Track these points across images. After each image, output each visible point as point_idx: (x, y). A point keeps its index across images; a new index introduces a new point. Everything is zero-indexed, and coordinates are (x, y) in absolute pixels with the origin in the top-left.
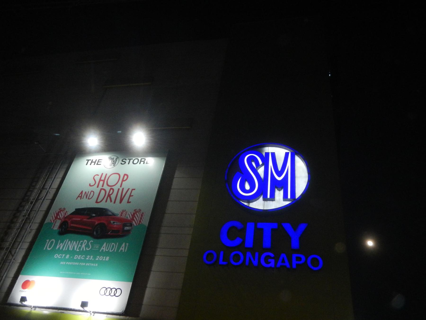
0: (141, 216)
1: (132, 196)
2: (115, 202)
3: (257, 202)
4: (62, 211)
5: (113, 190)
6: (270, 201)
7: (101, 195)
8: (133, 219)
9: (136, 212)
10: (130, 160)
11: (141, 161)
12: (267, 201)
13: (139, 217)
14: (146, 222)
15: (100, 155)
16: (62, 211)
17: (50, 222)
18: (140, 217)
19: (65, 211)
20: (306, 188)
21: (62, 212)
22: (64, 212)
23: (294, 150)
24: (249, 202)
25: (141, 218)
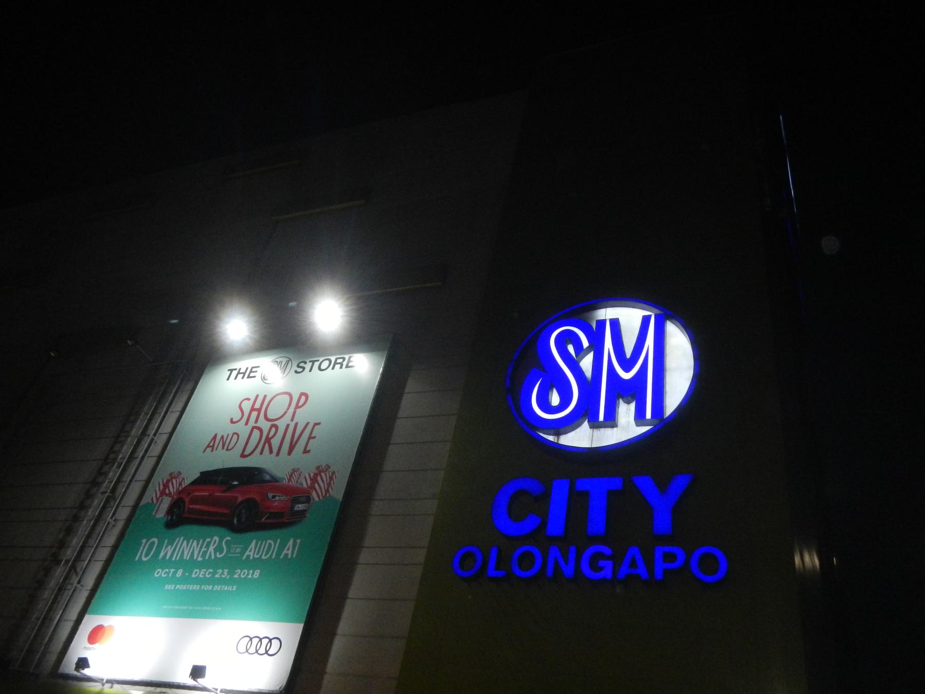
0: (330, 480)
1: (315, 437)
2: (278, 454)
5: (276, 427)
6: (606, 429)
7: (302, 436)
10: (313, 362)
11: (336, 363)
14: (338, 491)
25: (329, 485)
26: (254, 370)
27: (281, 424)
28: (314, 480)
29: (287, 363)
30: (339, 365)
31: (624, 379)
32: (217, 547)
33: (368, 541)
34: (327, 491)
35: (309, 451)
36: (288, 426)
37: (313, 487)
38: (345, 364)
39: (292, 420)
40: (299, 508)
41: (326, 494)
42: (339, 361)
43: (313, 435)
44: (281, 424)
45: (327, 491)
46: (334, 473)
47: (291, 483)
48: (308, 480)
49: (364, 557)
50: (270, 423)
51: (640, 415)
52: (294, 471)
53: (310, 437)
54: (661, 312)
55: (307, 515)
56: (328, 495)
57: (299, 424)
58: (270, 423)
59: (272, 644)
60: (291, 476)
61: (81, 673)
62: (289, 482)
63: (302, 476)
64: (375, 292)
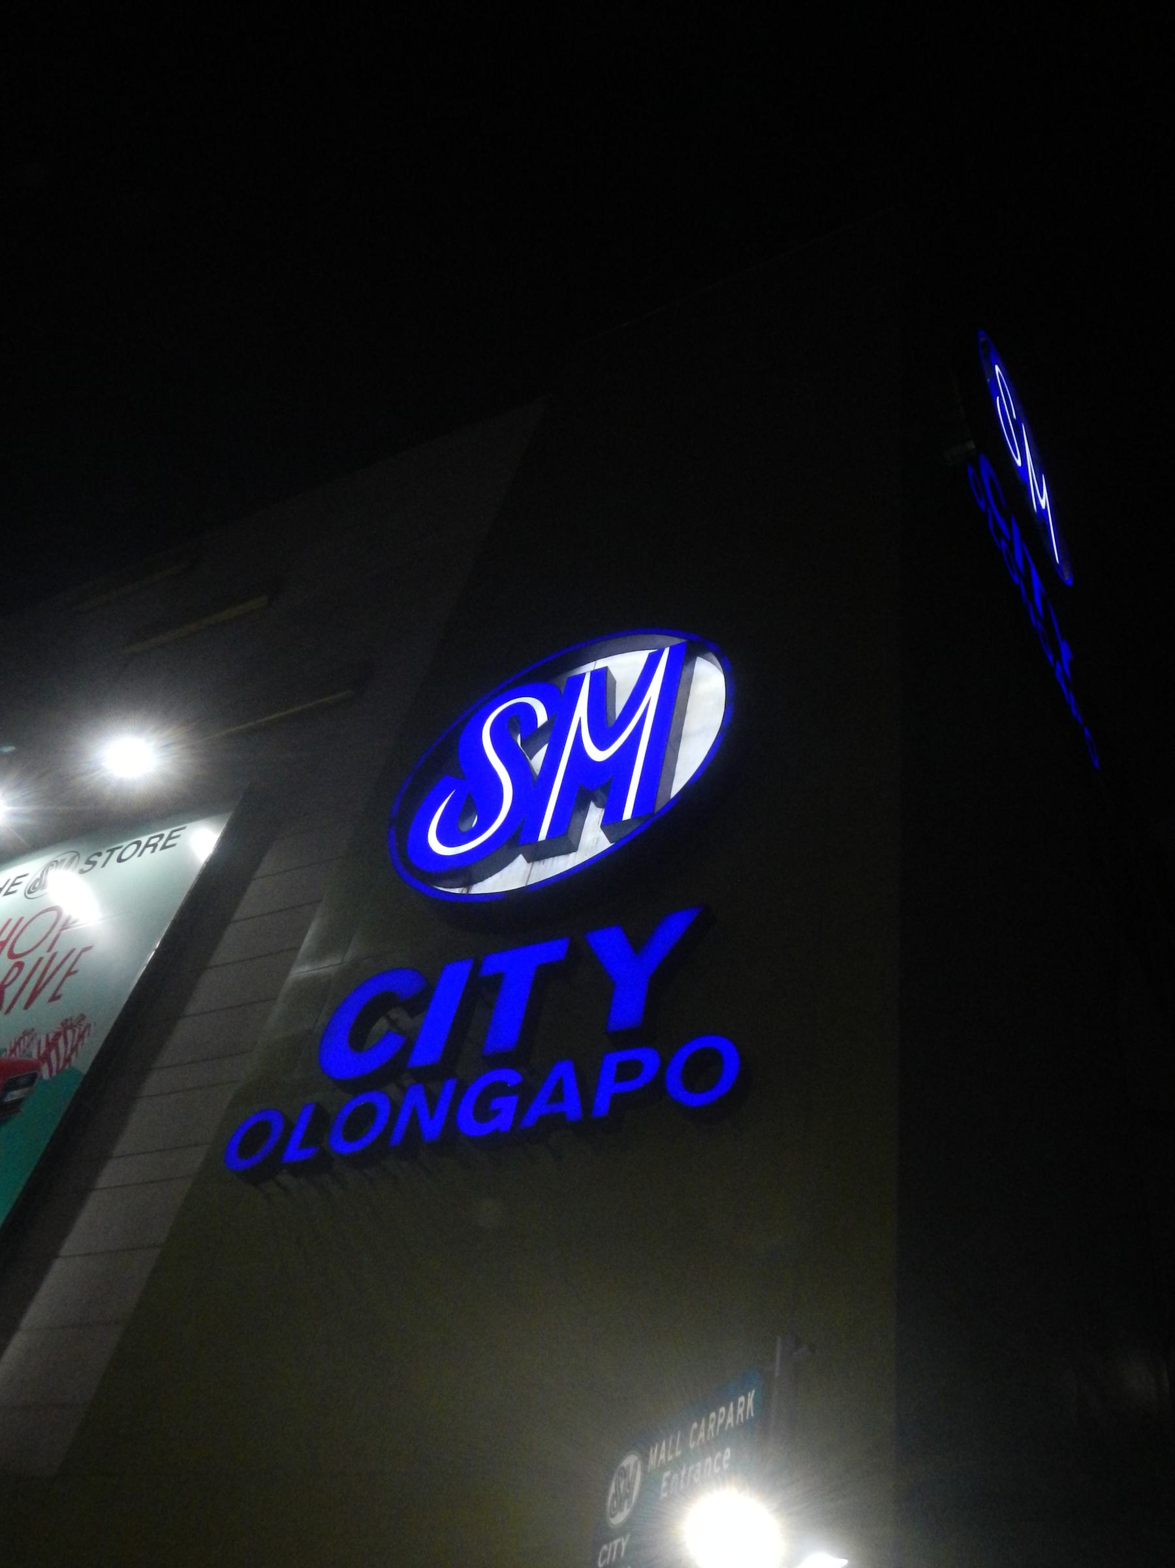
0: (79, 1041)
1: (76, 972)
2: (8, 1011)
3: (501, 876)
4: (72, 1027)
5: (20, 965)
6: (556, 858)
7: (55, 977)
8: (45, 1058)
9: (67, 1025)
10: (112, 851)
11: (147, 846)
12: (542, 862)
13: (70, 1044)
14: (83, 1062)
15: (24, 862)
16: (72, 1027)
17: (370, 959)
18: (42, 1052)
19: (84, 1023)
20: (589, 757)
21: (69, 1033)
22: (77, 1030)
23: (659, 812)
24: (469, 883)
25: (74, 1049)
26: (17, 881)
27: (29, 961)
28: (52, 1044)
29: (73, 858)
30: (152, 848)
31: (602, 762)
32: (599, 1551)
33: (124, 1145)
34: (68, 1060)
35: (59, 997)
36: (40, 960)
37: (45, 1058)
38: (160, 844)
39: (49, 950)
40: (12, 1096)
41: (64, 1066)
42: (153, 841)
43: (59, 993)
44: (29, 961)
45: (68, 1060)
46: (89, 1026)
47: (13, 1056)
48: (43, 1044)
49: (108, 1177)
50: (13, 962)
51: (611, 820)
52: (26, 1033)
53: (69, 973)
54: (683, 640)
55: (22, 1109)
56: (67, 1067)
57: (58, 955)
58: (13, 962)
59: (92, 870)
60: (18, 1044)
61: (1046, 507)
62: (10, 1054)
63: (35, 1042)
64: (232, 730)
